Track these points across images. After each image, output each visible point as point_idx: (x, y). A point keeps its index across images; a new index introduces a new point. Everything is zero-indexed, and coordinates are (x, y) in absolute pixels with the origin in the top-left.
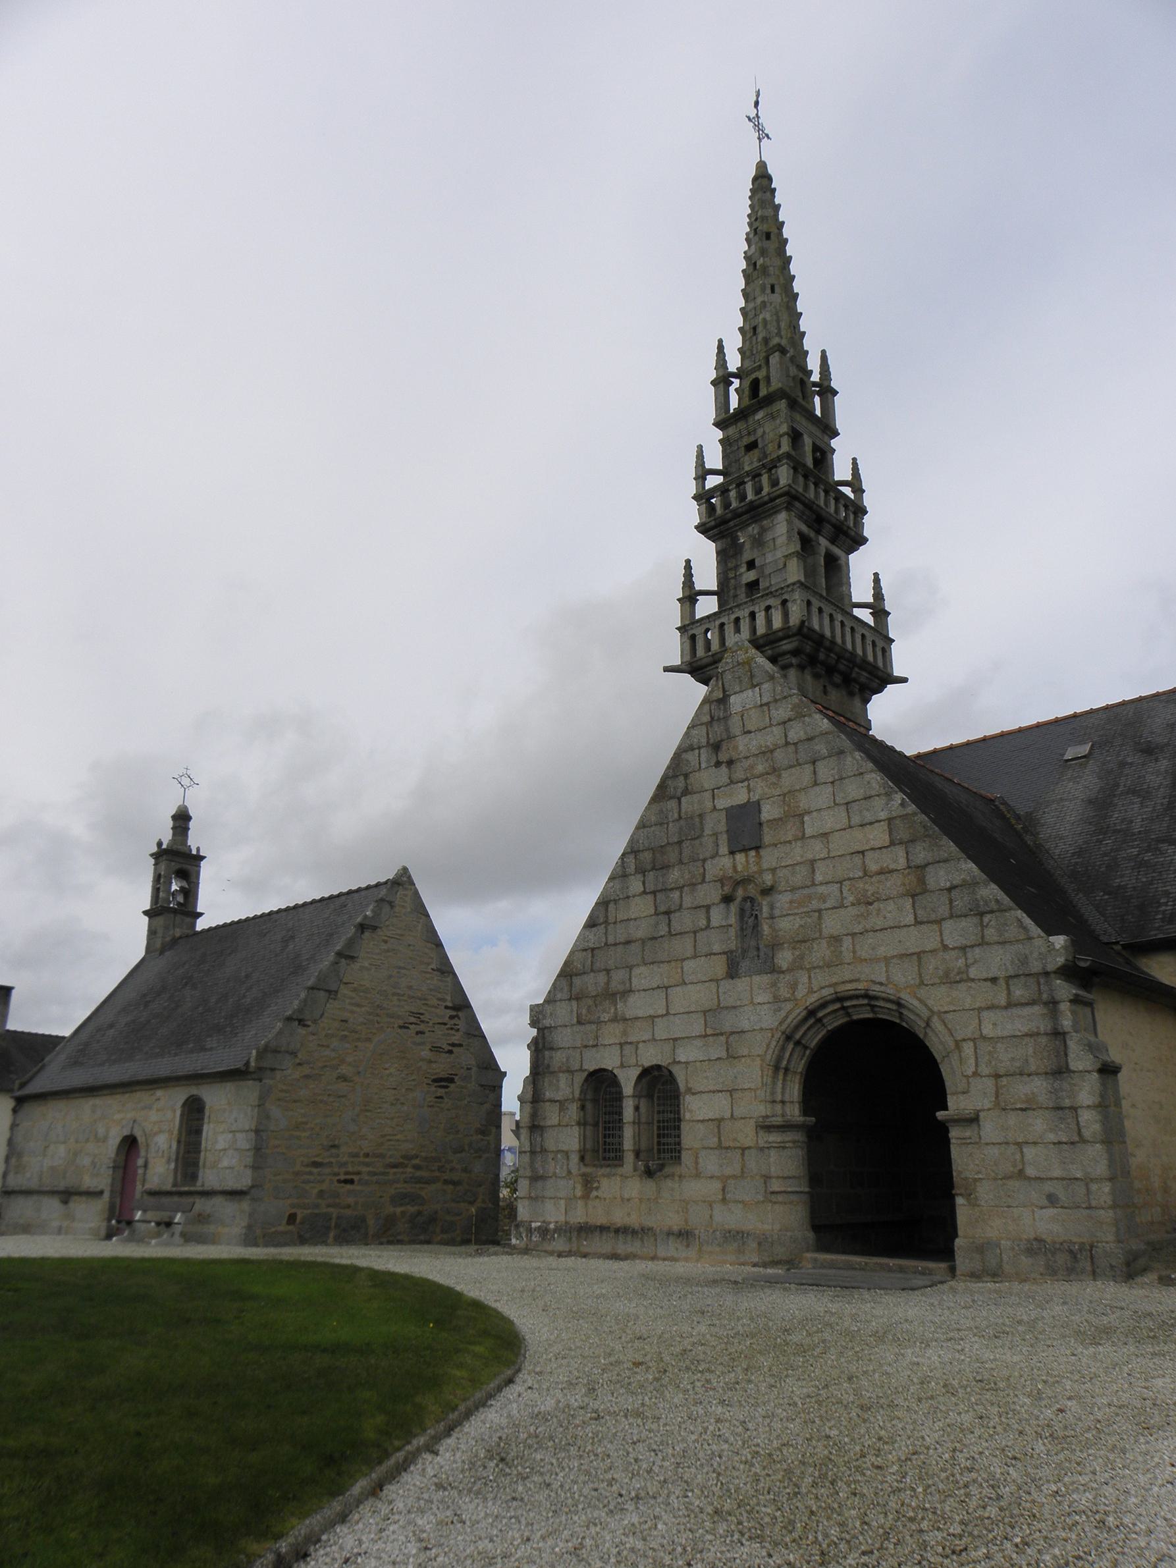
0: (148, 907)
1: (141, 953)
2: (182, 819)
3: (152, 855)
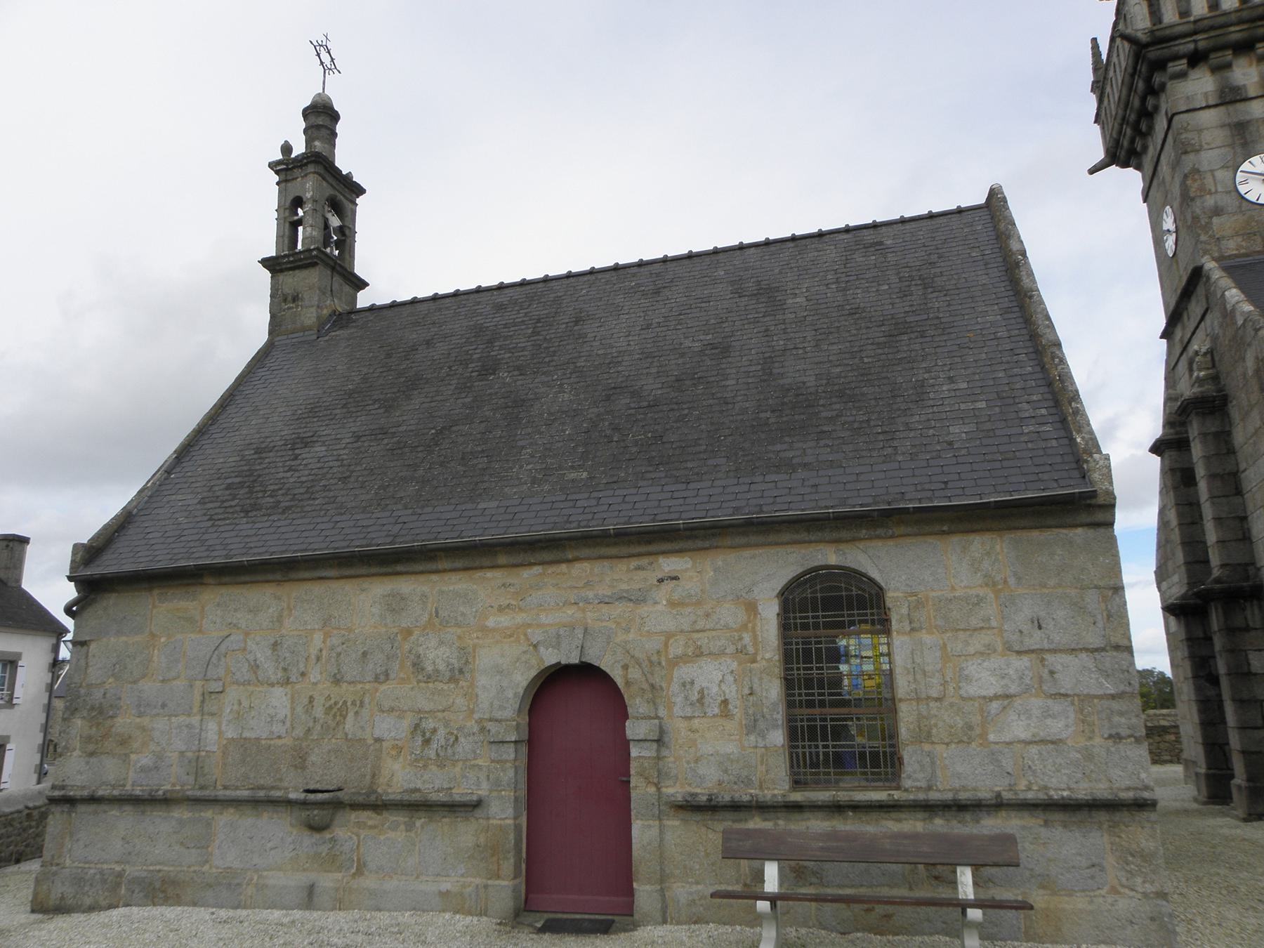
0: (271, 252)
1: (258, 335)
2: (321, 117)
3: (272, 165)
